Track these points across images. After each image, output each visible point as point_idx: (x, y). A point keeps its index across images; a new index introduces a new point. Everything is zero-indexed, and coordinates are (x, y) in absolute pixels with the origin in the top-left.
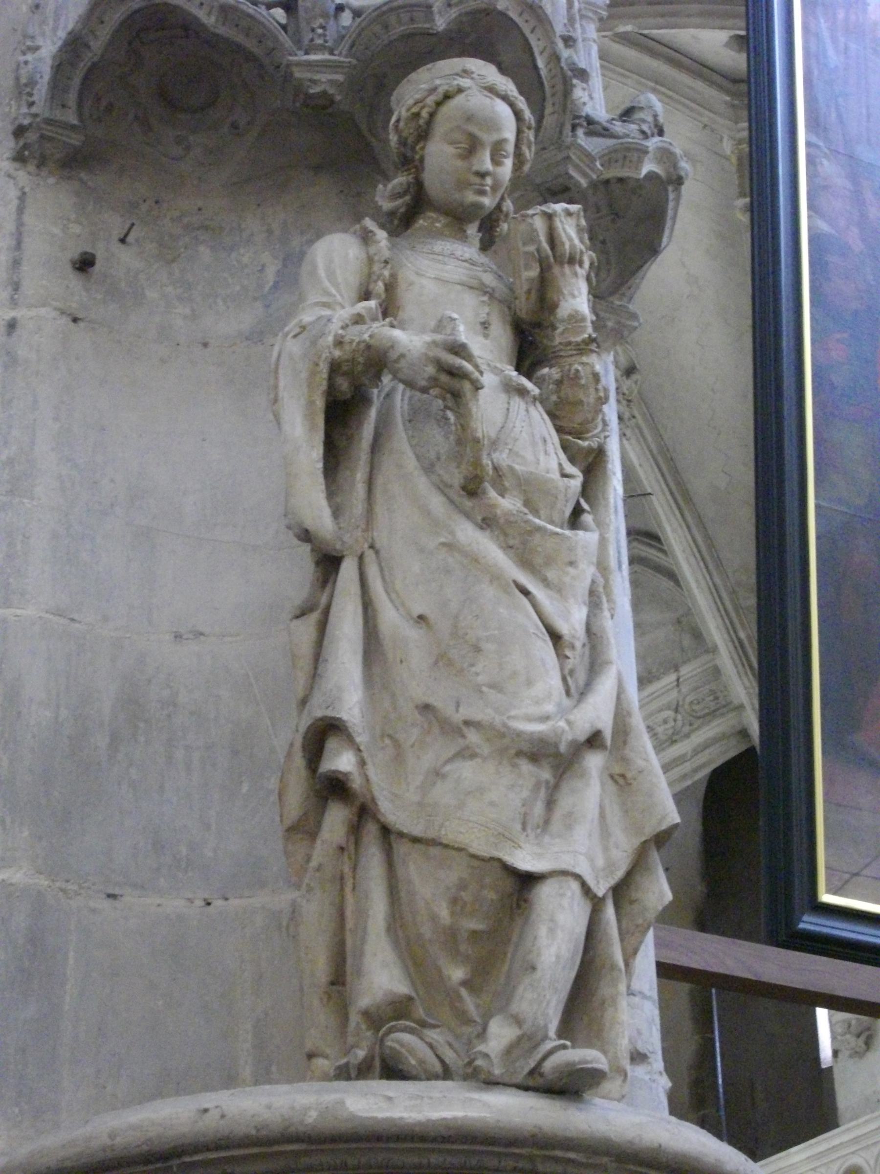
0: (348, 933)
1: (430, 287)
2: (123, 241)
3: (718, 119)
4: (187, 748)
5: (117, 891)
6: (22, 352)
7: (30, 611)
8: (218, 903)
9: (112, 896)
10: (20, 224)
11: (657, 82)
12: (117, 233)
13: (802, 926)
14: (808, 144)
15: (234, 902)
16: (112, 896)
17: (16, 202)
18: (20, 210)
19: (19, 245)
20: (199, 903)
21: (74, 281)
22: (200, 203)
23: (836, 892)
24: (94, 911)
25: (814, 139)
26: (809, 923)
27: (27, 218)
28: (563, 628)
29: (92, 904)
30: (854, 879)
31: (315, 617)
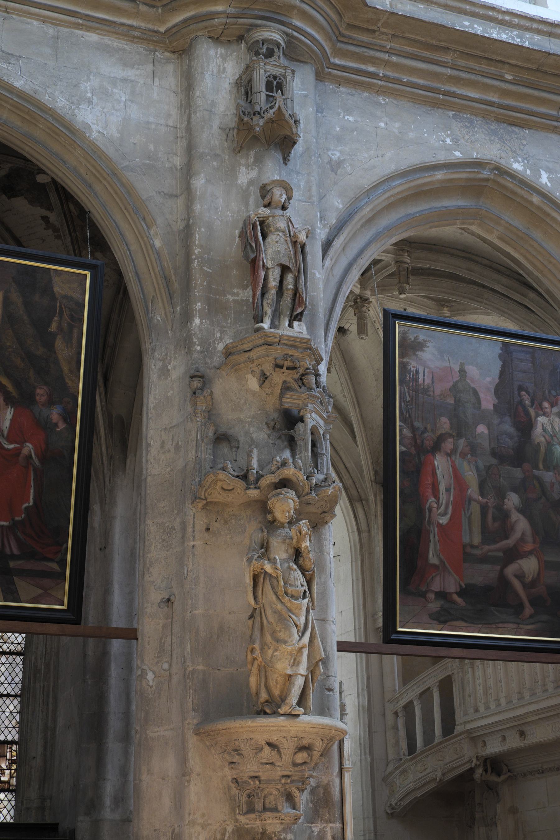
0: (305, 615)
1: (275, 544)
2: (216, 521)
3: (433, 311)
4: (232, 637)
5: (219, 668)
6: (196, 553)
7: (200, 611)
8: (239, 670)
9: (219, 670)
10: (194, 521)
11: (411, 302)
12: (215, 520)
13: (392, 637)
14: (400, 426)
15: (242, 669)
16: (219, 670)
17: (193, 516)
18: (194, 518)
19: (194, 527)
20: (235, 670)
21: (206, 534)
22: (232, 509)
23: (402, 628)
24: (215, 673)
25: (401, 424)
26: (394, 637)
27: (195, 520)
28: (298, 623)
29: (215, 671)
30: (408, 623)
31: (252, 619)
